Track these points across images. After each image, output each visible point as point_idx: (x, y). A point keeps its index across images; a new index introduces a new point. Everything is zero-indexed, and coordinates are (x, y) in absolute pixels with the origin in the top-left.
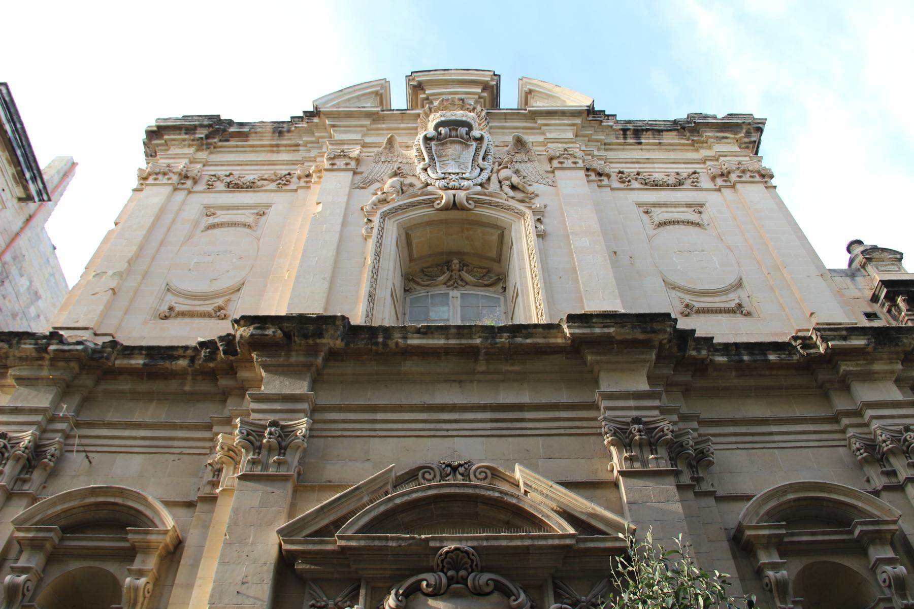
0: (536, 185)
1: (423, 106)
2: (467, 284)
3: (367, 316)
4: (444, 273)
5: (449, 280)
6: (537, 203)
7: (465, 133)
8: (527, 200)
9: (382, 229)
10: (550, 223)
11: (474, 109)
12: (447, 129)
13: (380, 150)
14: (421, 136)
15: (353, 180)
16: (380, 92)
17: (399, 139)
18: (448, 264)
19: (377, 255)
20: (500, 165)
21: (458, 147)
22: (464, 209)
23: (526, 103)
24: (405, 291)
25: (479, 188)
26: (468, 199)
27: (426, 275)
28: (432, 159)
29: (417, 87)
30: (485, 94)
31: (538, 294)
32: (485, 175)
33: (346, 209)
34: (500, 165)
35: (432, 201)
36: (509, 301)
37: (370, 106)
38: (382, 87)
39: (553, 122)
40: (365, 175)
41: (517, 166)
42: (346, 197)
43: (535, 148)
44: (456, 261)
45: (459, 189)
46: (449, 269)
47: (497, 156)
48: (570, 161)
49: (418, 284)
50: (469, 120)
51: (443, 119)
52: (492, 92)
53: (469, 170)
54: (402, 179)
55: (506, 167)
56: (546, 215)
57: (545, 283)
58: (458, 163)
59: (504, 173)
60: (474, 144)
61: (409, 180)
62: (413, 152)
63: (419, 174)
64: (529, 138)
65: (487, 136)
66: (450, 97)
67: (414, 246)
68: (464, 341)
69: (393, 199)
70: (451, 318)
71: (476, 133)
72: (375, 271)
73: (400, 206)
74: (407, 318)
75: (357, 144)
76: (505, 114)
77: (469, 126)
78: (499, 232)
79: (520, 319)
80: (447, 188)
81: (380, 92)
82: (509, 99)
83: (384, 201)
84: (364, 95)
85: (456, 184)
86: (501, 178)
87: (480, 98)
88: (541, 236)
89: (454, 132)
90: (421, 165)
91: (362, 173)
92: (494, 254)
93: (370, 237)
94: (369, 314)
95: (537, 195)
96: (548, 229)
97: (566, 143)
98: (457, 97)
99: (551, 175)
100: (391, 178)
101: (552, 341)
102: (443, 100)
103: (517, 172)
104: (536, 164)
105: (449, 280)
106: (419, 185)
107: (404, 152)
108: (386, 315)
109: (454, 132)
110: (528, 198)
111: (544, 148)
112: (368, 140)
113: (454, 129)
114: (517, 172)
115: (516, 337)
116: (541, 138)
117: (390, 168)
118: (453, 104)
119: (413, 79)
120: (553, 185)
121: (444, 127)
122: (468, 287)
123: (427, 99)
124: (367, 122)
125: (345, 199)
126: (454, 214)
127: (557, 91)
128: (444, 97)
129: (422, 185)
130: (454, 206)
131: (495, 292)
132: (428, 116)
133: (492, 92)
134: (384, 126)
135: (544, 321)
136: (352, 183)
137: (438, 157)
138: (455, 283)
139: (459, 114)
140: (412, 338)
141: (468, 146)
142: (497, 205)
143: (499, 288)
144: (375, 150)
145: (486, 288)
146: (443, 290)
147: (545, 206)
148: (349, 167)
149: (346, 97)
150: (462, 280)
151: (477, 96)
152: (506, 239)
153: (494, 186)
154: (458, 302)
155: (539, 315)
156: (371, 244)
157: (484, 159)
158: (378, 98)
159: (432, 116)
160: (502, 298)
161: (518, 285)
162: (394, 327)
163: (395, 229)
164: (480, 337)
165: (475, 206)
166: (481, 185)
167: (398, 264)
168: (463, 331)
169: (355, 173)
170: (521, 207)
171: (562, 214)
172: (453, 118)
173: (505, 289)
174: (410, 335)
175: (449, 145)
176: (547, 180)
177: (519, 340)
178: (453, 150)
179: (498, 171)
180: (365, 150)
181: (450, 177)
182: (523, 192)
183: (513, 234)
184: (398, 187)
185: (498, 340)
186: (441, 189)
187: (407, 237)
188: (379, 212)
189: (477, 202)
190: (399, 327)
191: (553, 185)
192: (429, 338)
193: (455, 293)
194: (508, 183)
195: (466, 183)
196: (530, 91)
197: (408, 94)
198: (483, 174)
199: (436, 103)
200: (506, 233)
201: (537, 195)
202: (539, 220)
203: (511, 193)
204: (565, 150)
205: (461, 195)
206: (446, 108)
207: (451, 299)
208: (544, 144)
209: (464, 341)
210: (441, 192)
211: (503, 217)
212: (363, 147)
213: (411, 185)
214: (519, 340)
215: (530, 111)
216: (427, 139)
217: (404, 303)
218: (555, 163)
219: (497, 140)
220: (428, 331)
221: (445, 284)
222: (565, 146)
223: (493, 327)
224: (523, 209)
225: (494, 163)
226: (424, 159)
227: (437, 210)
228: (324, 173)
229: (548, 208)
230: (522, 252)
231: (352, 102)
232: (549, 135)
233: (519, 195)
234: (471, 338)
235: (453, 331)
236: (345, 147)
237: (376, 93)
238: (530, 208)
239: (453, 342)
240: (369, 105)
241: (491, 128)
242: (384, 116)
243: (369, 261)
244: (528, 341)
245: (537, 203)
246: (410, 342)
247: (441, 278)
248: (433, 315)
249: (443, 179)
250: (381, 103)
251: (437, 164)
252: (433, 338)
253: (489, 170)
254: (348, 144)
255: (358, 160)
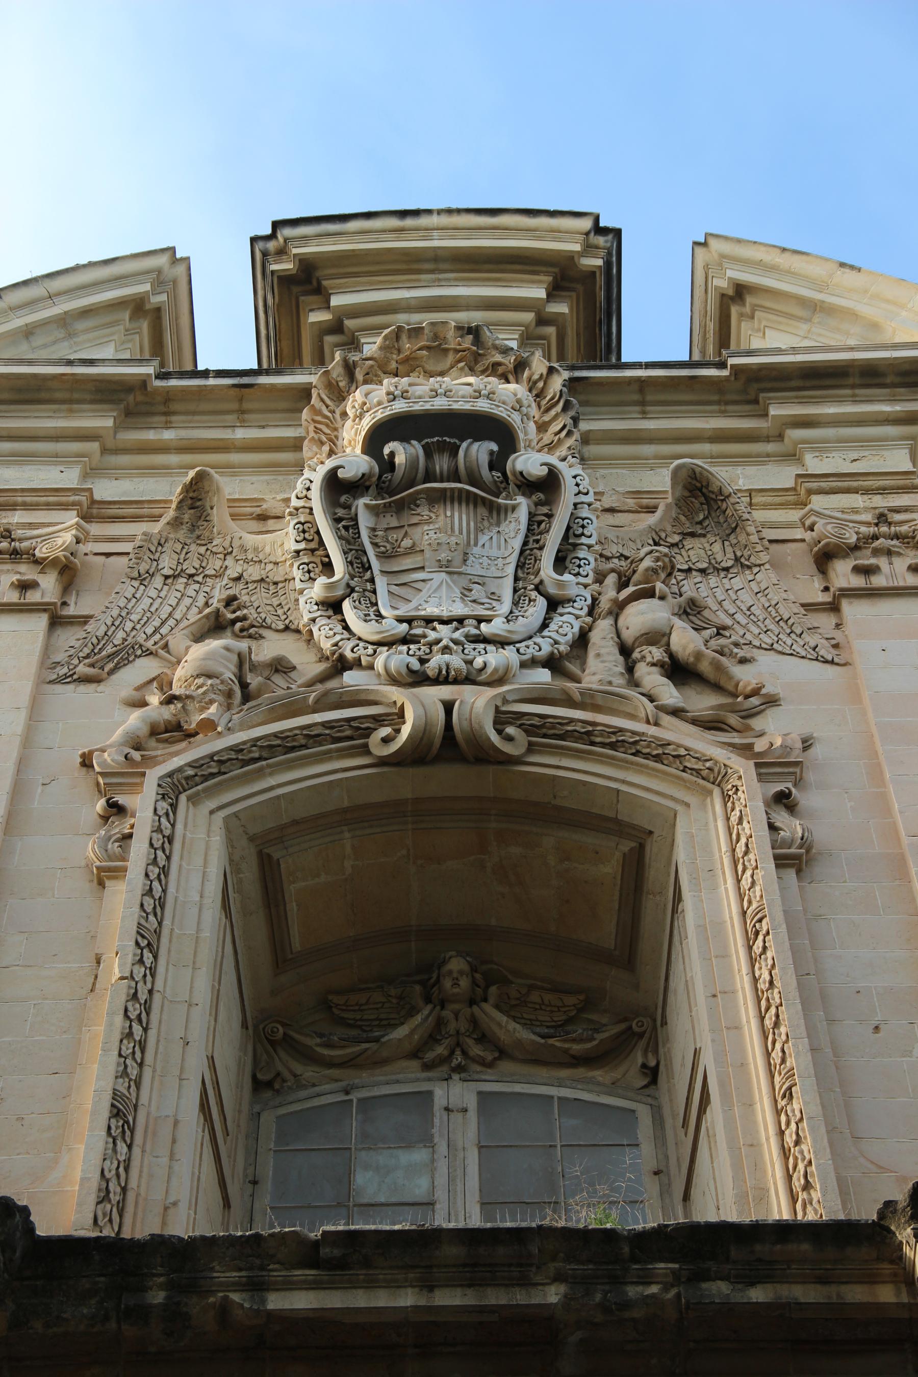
0: (765, 660)
1: (320, 359)
2: (503, 1053)
3: (104, 1197)
4: (412, 1012)
5: (433, 1038)
6: (775, 730)
7: (484, 460)
8: (733, 720)
9: (164, 841)
10: (827, 812)
11: (521, 366)
12: (416, 448)
13: (155, 528)
14: (316, 475)
15: (47, 649)
16: (154, 300)
17: (230, 487)
18: (426, 978)
19: (148, 943)
20: (623, 584)
21: (458, 518)
22: (479, 754)
23: (724, 339)
24: (258, 1085)
25: (543, 676)
26: (501, 719)
27: (342, 1022)
28: (359, 563)
29: (297, 280)
30: (561, 308)
31: (789, 1094)
32: (566, 626)
33: (22, 764)
34: (623, 584)
35: (359, 731)
36: (672, 1124)
37: (112, 354)
38: (159, 280)
39: (831, 410)
40: (96, 628)
41: (690, 587)
42: (23, 715)
43: (759, 515)
44: (456, 964)
45: (468, 680)
46: (433, 995)
47: (613, 549)
48: (900, 565)
49: (310, 1058)
50: (501, 412)
51: (400, 406)
52: (590, 297)
53: (505, 606)
54: (243, 645)
55: (649, 594)
56: (810, 776)
57: (814, 1050)
58: (460, 573)
59: (641, 616)
60: (523, 504)
61: (271, 647)
62: (286, 539)
63: (305, 622)
64: (737, 477)
65: (568, 471)
66: (425, 319)
67: (292, 907)
68: (496, 1297)
69: (208, 725)
70: (441, 1195)
71: (529, 462)
72: (139, 1010)
73: (237, 749)
74: (265, 1199)
75: (65, 507)
76: (642, 383)
77: (502, 434)
78: (627, 846)
79: (720, 1200)
80: (417, 678)
81: (154, 300)
82: (655, 326)
83: (172, 732)
84: (86, 313)
85: (456, 661)
86: (629, 635)
87: (542, 320)
88: (793, 860)
89: (439, 464)
90: (318, 589)
91: (84, 620)
92: (606, 933)
93: (118, 873)
94: (112, 1191)
95: (772, 701)
96: (822, 835)
97: (882, 491)
98: (454, 318)
99: (826, 621)
100: (198, 638)
101: (856, 1294)
102: (398, 333)
103: (691, 610)
104: (766, 577)
105: (433, 1038)
106: (308, 665)
107: (251, 540)
108: (182, 1190)
109: (439, 464)
110: (736, 711)
111: (794, 515)
112: (106, 490)
113: (442, 447)
114: (691, 610)
115: (706, 1277)
116: (782, 476)
117: (190, 604)
118: (438, 348)
119: (281, 252)
120: (835, 657)
121: (404, 439)
122: (506, 1066)
123: (336, 328)
124: (102, 421)
125: (17, 723)
126: (445, 780)
127: (845, 292)
128: (402, 319)
129: (322, 667)
130: (447, 746)
131: (613, 1088)
132: (340, 396)
133: (590, 297)
134: (168, 435)
135: (818, 1208)
136: (47, 662)
137: (384, 556)
138: (457, 1050)
139: (459, 390)
140: (288, 1286)
141: (497, 513)
142: (618, 744)
143: (630, 1069)
144: (138, 529)
145: (581, 1072)
146: (407, 1079)
147: (807, 744)
148: (33, 597)
149: (18, 322)
150: (483, 1038)
151: (529, 317)
152: (652, 873)
153: (601, 668)
154: (468, 1131)
155: (798, 1182)
156: (123, 900)
157: (560, 563)
158: (145, 325)
159: (358, 396)
160: (644, 1113)
161: (707, 1060)
162: (211, 1241)
163: (217, 840)
164: (558, 1278)
165: (531, 748)
166: (552, 663)
167: (230, 977)
168: (487, 1252)
169: (57, 621)
170: (707, 746)
171: (876, 774)
172: (440, 404)
173: (652, 1074)
174: (277, 1273)
175: (424, 511)
176: (812, 640)
177: (719, 1289)
178: (438, 528)
179: (618, 608)
180: (95, 529)
181: (448, 627)
182: (717, 687)
183: (681, 855)
184: (229, 674)
185: (633, 1291)
186: (394, 680)
187: (265, 865)
188: (153, 775)
189: (541, 731)
190: (231, 1241)
191: (835, 657)
192: (353, 1285)
193: (458, 1093)
194: (657, 653)
195: (494, 658)
196: (740, 291)
197: (261, 311)
198: (557, 621)
199: (372, 346)
200: (653, 849)
201: (772, 701)
202: (783, 800)
203: (670, 694)
204: (882, 518)
205: (476, 703)
206: (409, 366)
207: (439, 1116)
208: (795, 497)
209: (496, 1297)
210: (396, 694)
211: (640, 784)
212: (86, 517)
213: (280, 666)
214: (719, 1289)
215: (737, 370)
216: (338, 488)
217: (254, 1136)
218: (842, 573)
219: (617, 487)
220: (350, 1256)
221: (415, 1054)
222: (880, 502)
223: (610, 1235)
224: (720, 754)
225: (600, 578)
226: (328, 567)
227: (383, 762)
228: (849, 608)
229: (817, 751)
230: (720, 926)
231: (38, 341)
232: (814, 464)
233: (703, 702)
234: (525, 1283)
235: (452, 1251)
236: (17, 517)
237: (137, 307)
238: (746, 750)
239: (449, 1298)
240: (108, 352)
241: (586, 439)
242: (169, 397)
243: (115, 969)
244: (758, 1295)
245: (775, 730)
246: (276, 1302)
247: (401, 1032)
248: (367, 1183)
249: (405, 640)
250: (157, 347)
251: (381, 584)
252: (371, 1285)
253: (582, 606)
254: (27, 507)
255: (68, 572)
